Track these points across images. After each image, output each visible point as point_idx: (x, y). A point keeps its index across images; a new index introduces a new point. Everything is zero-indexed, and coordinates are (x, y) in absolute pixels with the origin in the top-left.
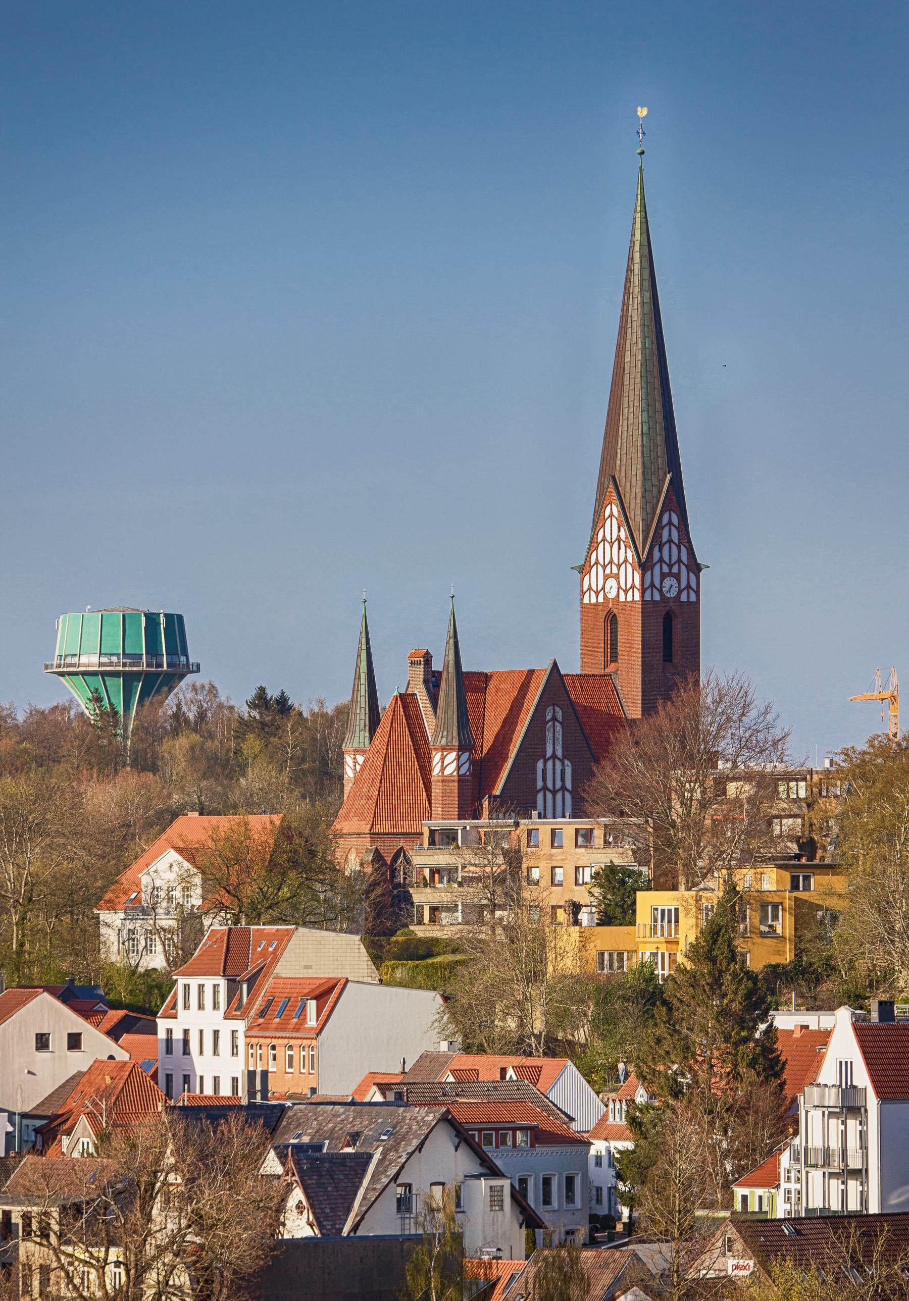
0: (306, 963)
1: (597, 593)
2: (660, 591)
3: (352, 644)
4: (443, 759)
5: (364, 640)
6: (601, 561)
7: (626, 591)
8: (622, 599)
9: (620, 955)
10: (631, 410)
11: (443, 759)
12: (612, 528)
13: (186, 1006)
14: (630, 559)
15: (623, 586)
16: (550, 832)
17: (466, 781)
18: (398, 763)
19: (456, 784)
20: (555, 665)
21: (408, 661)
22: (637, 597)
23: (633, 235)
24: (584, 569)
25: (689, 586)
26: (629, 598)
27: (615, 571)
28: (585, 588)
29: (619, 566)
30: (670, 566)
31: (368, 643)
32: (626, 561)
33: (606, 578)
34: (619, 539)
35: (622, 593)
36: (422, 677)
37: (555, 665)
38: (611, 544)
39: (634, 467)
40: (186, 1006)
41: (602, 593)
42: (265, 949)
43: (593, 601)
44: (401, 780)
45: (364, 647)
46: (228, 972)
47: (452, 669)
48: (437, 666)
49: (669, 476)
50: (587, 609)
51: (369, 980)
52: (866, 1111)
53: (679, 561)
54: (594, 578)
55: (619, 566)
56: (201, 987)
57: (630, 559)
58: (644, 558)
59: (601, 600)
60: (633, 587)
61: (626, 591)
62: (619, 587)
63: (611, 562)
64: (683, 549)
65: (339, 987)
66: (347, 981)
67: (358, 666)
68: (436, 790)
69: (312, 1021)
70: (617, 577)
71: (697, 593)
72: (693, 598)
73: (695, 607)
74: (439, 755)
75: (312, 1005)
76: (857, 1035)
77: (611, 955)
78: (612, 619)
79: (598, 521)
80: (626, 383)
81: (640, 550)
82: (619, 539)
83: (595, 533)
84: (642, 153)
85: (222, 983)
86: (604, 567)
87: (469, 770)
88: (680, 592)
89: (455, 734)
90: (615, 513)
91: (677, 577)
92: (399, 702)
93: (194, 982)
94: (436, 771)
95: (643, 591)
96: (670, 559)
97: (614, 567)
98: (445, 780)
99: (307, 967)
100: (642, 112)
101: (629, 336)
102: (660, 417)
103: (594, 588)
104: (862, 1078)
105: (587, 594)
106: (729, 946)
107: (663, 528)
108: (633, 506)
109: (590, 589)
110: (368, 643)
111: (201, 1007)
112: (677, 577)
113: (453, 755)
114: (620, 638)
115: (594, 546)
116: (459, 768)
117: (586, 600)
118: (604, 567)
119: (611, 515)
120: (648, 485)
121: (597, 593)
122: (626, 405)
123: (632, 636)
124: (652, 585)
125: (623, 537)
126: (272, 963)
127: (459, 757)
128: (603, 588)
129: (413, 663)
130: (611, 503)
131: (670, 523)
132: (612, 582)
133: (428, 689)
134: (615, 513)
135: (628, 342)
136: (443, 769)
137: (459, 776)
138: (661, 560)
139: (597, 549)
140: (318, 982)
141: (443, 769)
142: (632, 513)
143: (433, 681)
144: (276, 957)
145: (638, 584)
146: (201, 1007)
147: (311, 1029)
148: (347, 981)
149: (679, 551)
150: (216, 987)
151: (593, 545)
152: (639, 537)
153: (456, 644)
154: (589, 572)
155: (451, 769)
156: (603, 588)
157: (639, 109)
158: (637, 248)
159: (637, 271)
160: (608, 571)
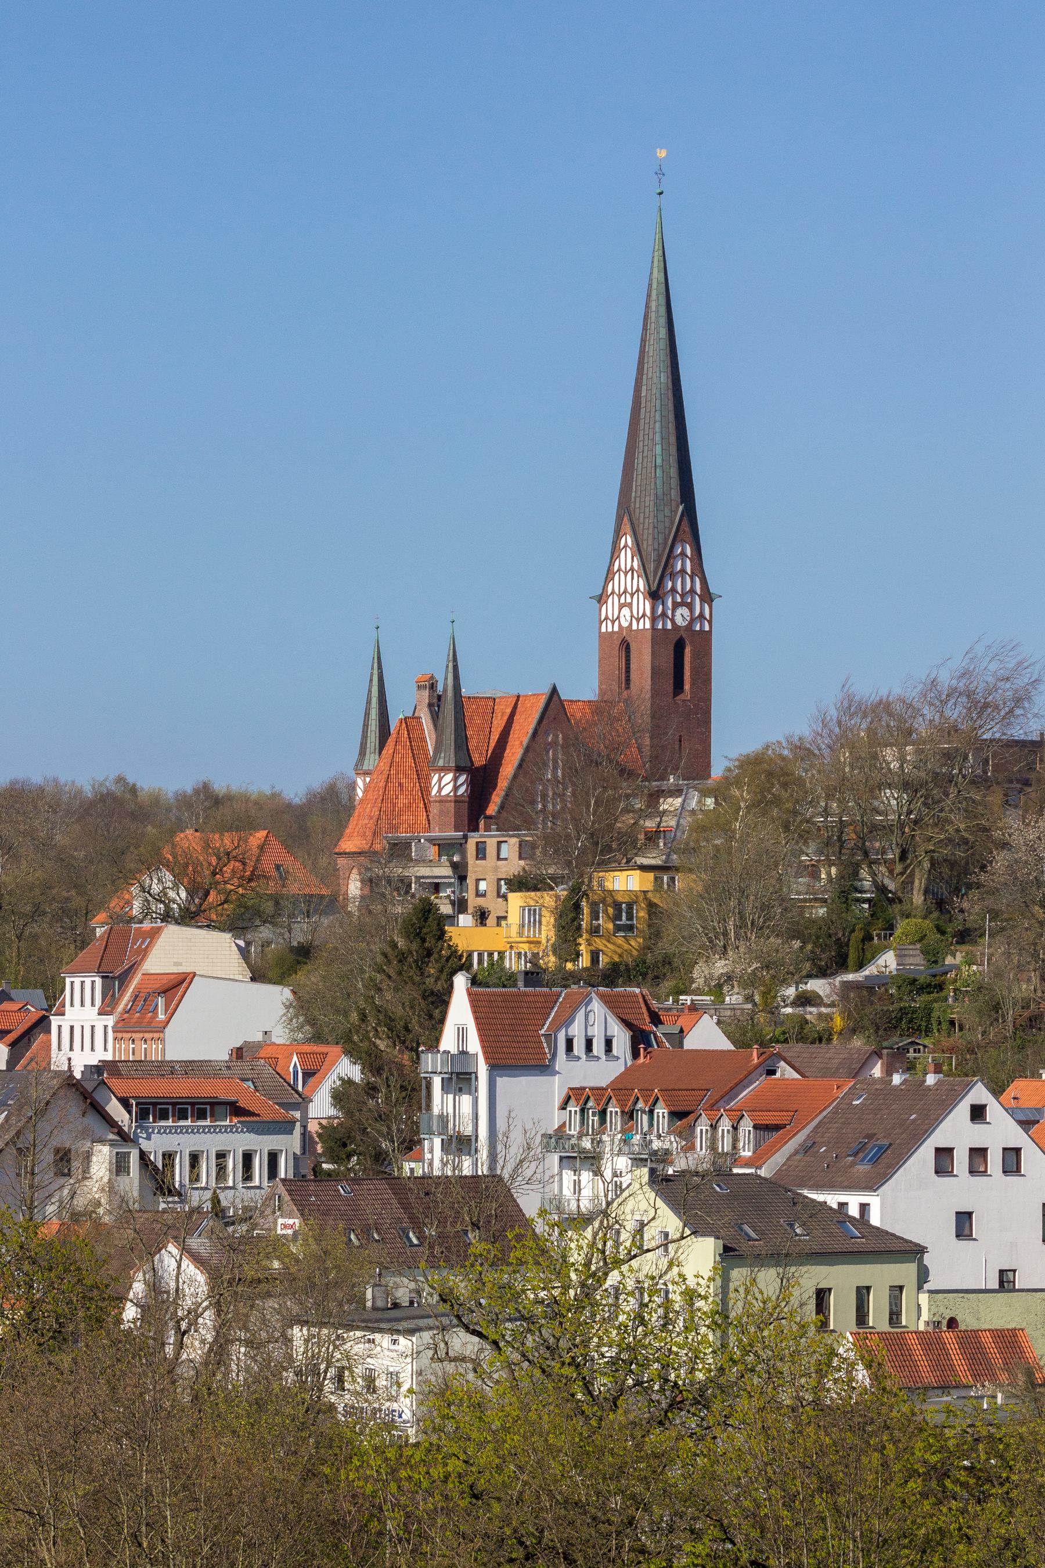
0: (175, 960)
1: (613, 622)
2: (673, 621)
3: (365, 669)
4: (440, 779)
5: (376, 665)
6: (617, 591)
7: (638, 620)
8: (635, 627)
9: (490, 955)
10: (646, 443)
11: (440, 779)
12: (627, 559)
13: (72, 1005)
14: (642, 588)
15: (635, 615)
16: (495, 845)
17: (462, 802)
18: (400, 784)
19: (453, 805)
20: (554, 691)
21: (415, 686)
22: (648, 626)
23: (651, 273)
24: (601, 599)
25: (702, 616)
26: (641, 627)
27: (629, 600)
28: (603, 618)
29: (632, 595)
30: (682, 596)
31: (380, 667)
32: (638, 590)
33: (621, 606)
34: (632, 569)
35: (634, 622)
36: (427, 701)
37: (554, 691)
38: (626, 574)
39: (647, 498)
40: (72, 1005)
41: (617, 622)
42: (140, 946)
43: (610, 629)
44: (402, 801)
45: (376, 672)
46: (103, 968)
47: (450, 693)
48: (440, 688)
49: (681, 508)
50: (605, 638)
51: (240, 978)
52: (477, 1078)
53: (692, 591)
54: (610, 608)
55: (632, 595)
56: (83, 983)
57: (642, 588)
58: (654, 588)
59: (616, 629)
60: (644, 615)
61: (638, 620)
62: (632, 616)
63: (625, 592)
64: (697, 580)
65: (187, 981)
66: (195, 974)
67: (370, 691)
68: (434, 810)
69: (161, 1017)
70: (630, 605)
71: (710, 622)
72: (707, 628)
73: (706, 637)
74: (437, 776)
75: (161, 1001)
76: (471, 1001)
77: (480, 955)
78: (626, 647)
79: (615, 551)
80: (642, 416)
81: (651, 579)
82: (632, 569)
83: (611, 564)
84: (661, 193)
85: (98, 981)
86: (619, 596)
87: (466, 791)
88: (692, 620)
89: (452, 755)
90: (630, 543)
91: (690, 607)
92: (404, 725)
93: (77, 981)
94: (434, 792)
95: (654, 619)
96: (682, 589)
97: (628, 596)
98: (442, 801)
99: (179, 964)
100: (662, 154)
101: (645, 372)
102: (673, 450)
103: (610, 617)
104: (474, 1045)
105: (604, 624)
106: (439, 925)
107: (675, 558)
108: (645, 537)
109: (607, 618)
110: (380, 667)
111: (82, 1005)
112: (690, 607)
113: (450, 776)
114: (633, 666)
115: (610, 576)
116: (456, 788)
117: (603, 630)
118: (619, 596)
119: (626, 546)
120: (661, 516)
121: (613, 622)
122: (641, 438)
123: (643, 661)
124: (664, 614)
125: (636, 567)
126: (142, 960)
127: (455, 779)
128: (618, 617)
129: (419, 687)
130: (625, 534)
131: (683, 554)
132: (626, 611)
133: (431, 711)
134: (689, 552)
135: (645, 377)
136: (440, 789)
137: (455, 796)
138: (673, 590)
139: (613, 579)
140: (173, 977)
141: (440, 789)
142: (645, 543)
143: (435, 705)
144: (144, 953)
145: (648, 613)
146: (82, 1005)
147: (161, 1022)
148: (195, 974)
149: (692, 581)
150: (93, 982)
151: (609, 575)
152: (651, 567)
153: (456, 668)
154: (606, 602)
155: (447, 790)
156: (618, 617)
157: (658, 150)
158: (654, 286)
159: (654, 308)
160: (622, 600)
